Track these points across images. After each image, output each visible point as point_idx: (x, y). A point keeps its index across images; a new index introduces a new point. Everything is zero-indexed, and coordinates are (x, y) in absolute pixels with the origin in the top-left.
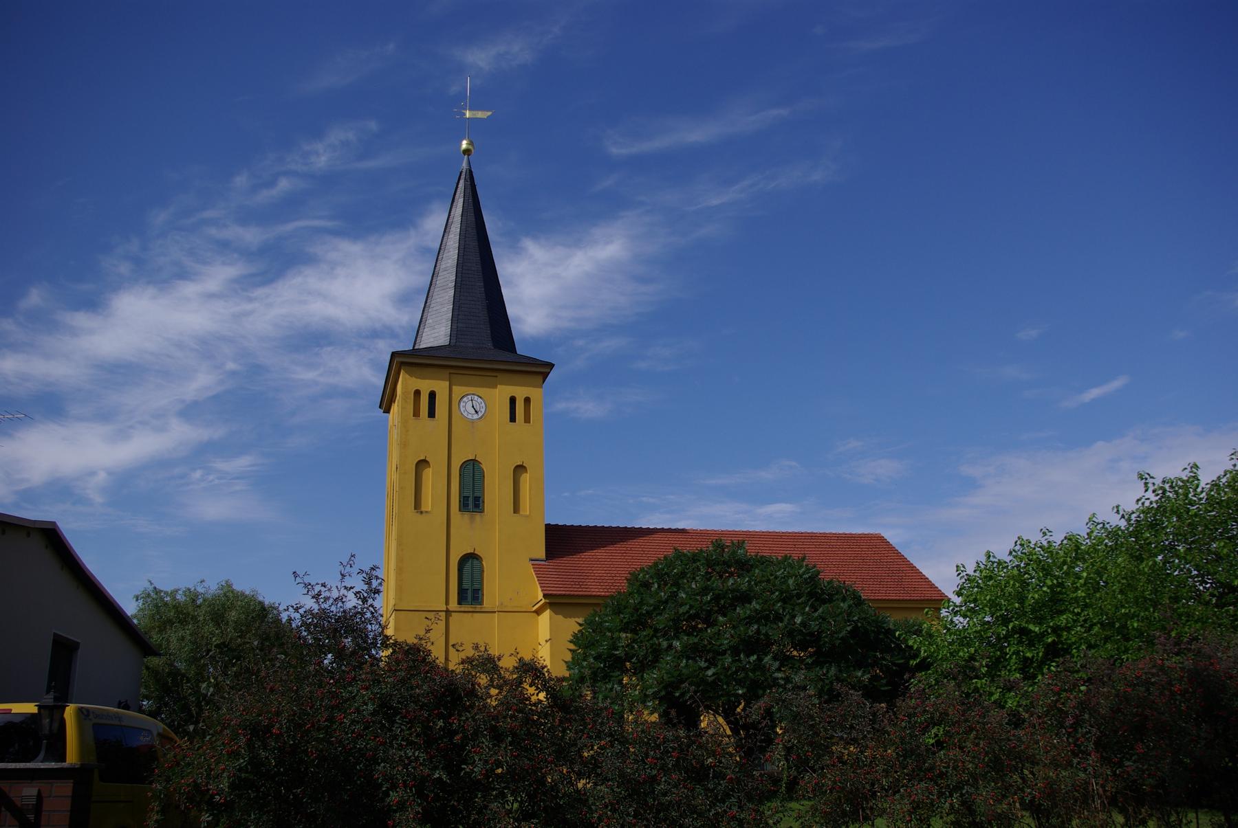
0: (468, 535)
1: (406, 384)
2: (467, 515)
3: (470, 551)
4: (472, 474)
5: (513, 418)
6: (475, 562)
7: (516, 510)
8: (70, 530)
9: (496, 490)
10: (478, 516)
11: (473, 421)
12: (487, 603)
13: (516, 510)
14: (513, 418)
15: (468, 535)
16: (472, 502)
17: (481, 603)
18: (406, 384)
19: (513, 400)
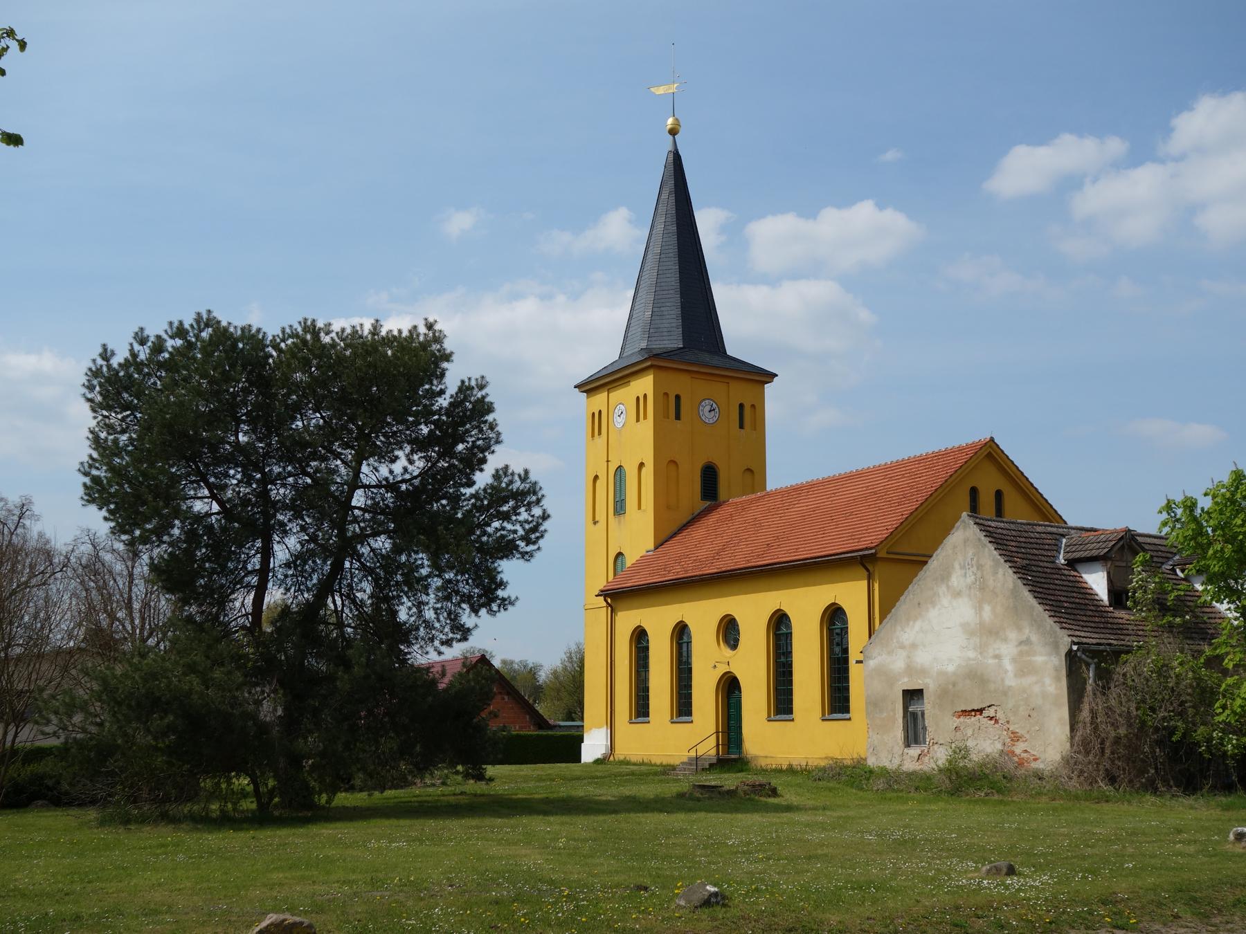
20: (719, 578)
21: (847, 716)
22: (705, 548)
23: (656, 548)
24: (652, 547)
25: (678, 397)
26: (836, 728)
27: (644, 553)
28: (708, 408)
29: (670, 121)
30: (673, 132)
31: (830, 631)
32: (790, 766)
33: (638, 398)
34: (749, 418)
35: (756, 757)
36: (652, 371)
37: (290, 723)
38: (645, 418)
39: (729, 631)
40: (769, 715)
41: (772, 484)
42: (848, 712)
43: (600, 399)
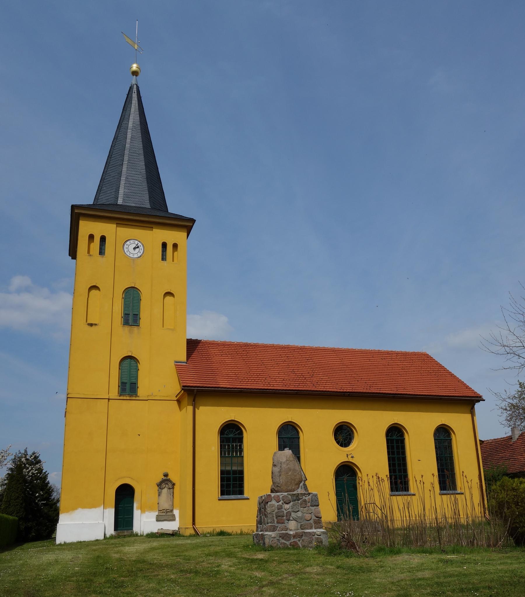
0: (128, 342)
1: (86, 227)
2: (127, 328)
3: (94, 284)
4: (132, 296)
5: (164, 258)
6: (133, 362)
7: (173, 261)
8: (443, 423)
9: (147, 310)
10: (135, 329)
11: (134, 259)
12: (142, 391)
13: (173, 261)
14: (164, 258)
15: (128, 342)
16: (131, 318)
17: (408, 491)
18: (86, 227)
19: (164, 245)
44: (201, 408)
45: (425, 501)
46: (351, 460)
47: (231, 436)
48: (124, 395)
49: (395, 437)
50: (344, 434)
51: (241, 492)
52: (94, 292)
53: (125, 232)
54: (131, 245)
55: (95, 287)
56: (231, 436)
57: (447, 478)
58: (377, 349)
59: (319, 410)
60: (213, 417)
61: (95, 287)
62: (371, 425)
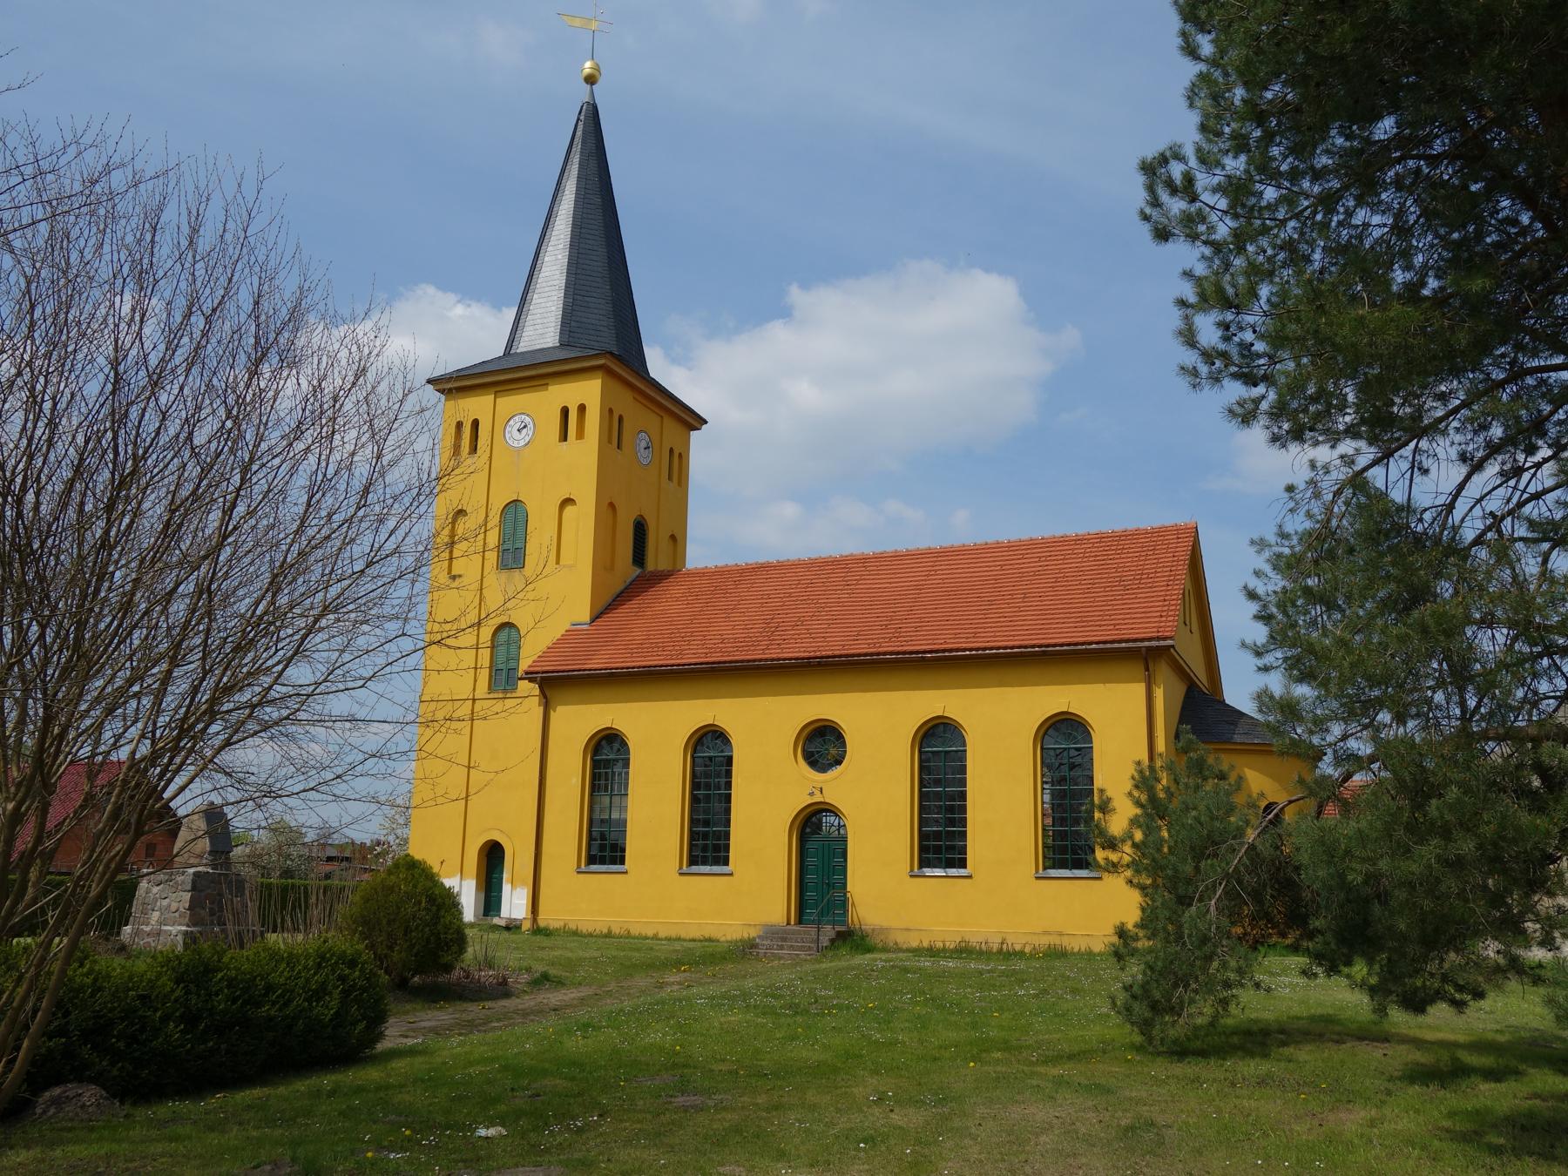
4: (514, 514)
11: (519, 450)
16: (512, 556)
20: (809, 665)
21: (724, 869)
22: (649, 632)
23: (594, 619)
24: (584, 615)
25: (621, 419)
26: (706, 886)
27: (568, 627)
28: (644, 444)
29: (588, 64)
30: (591, 80)
31: (596, 764)
32: (610, 931)
33: (459, 425)
34: (676, 466)
35: (883, 930)
36: (600, 374)
37: (1484, 881)
38: (580, 434)
39: (822, 745)
40: (579, 866)
41: (698, 556)
42: (622, 862)
43: (477, 406)
44: (560, 709)
45: (1007, 898)
46: (818, 798)
47: (607, 757)
48: (496, 691)
49: (939, 752)
50: (822, 745)
51: (725, 861)
52: (569, 509)
53: (508, 402)
54: (515, 423)
55: (568, 501)
56: (607, 757)
57: (707, 842)
58: (1025, 537)
59: (1099, 687)
60: (580, 721)
61: (568, 501)
62: (883, 723)
